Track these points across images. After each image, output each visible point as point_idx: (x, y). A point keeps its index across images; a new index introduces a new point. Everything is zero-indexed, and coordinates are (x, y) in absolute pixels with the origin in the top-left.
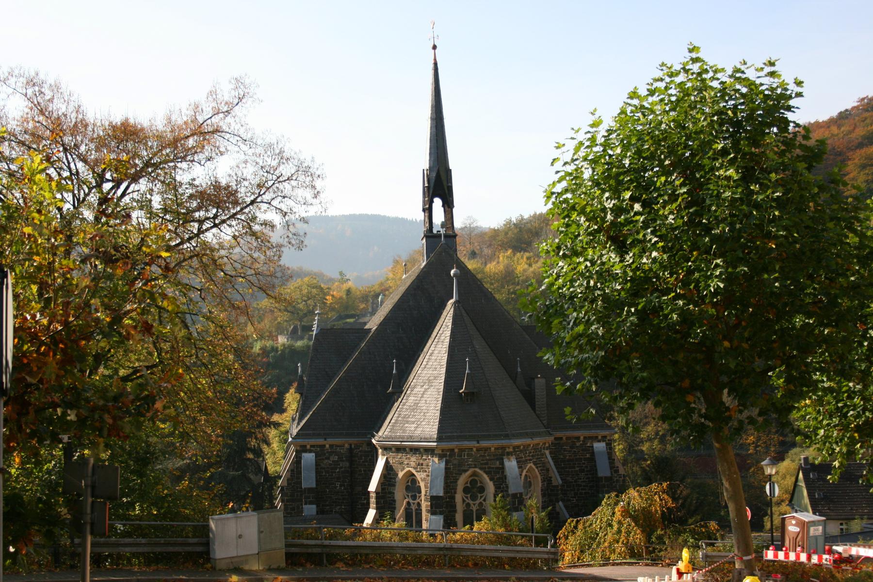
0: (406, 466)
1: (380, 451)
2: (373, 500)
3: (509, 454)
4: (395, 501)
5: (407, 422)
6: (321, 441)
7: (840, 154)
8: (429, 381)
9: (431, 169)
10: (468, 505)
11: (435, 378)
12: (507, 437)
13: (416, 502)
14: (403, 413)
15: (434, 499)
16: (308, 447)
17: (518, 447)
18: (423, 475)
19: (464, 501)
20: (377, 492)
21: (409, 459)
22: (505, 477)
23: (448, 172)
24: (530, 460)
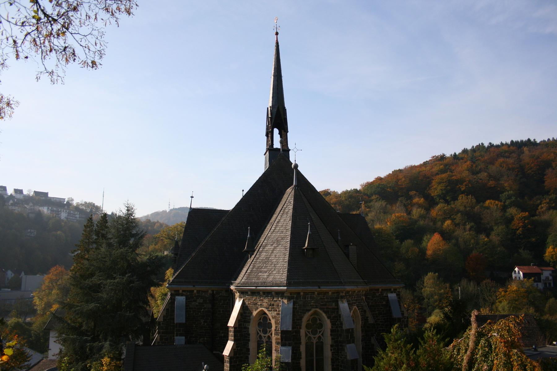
0: (261, 306)
1: (237, 295)
2: (231, 334)
3: (342, 297)
4: (249, 335)
5: (261, 272)
6: (190, 287)
7: (428, 178)
8: (277, 241)
9: (273, 107)
10: (310, 338)
11: (282, 239)
12: (341, 284)
13: (267, 335)
14: (257, 265)
15: (284, 333)
16: (181, 291)
17: (348, 292)
18: (274, 313)
19: (306, 335)
20: (235, 327)
21: (262, 300)
22: (340, 316)
23: (285, 110)
24: (355, 303)
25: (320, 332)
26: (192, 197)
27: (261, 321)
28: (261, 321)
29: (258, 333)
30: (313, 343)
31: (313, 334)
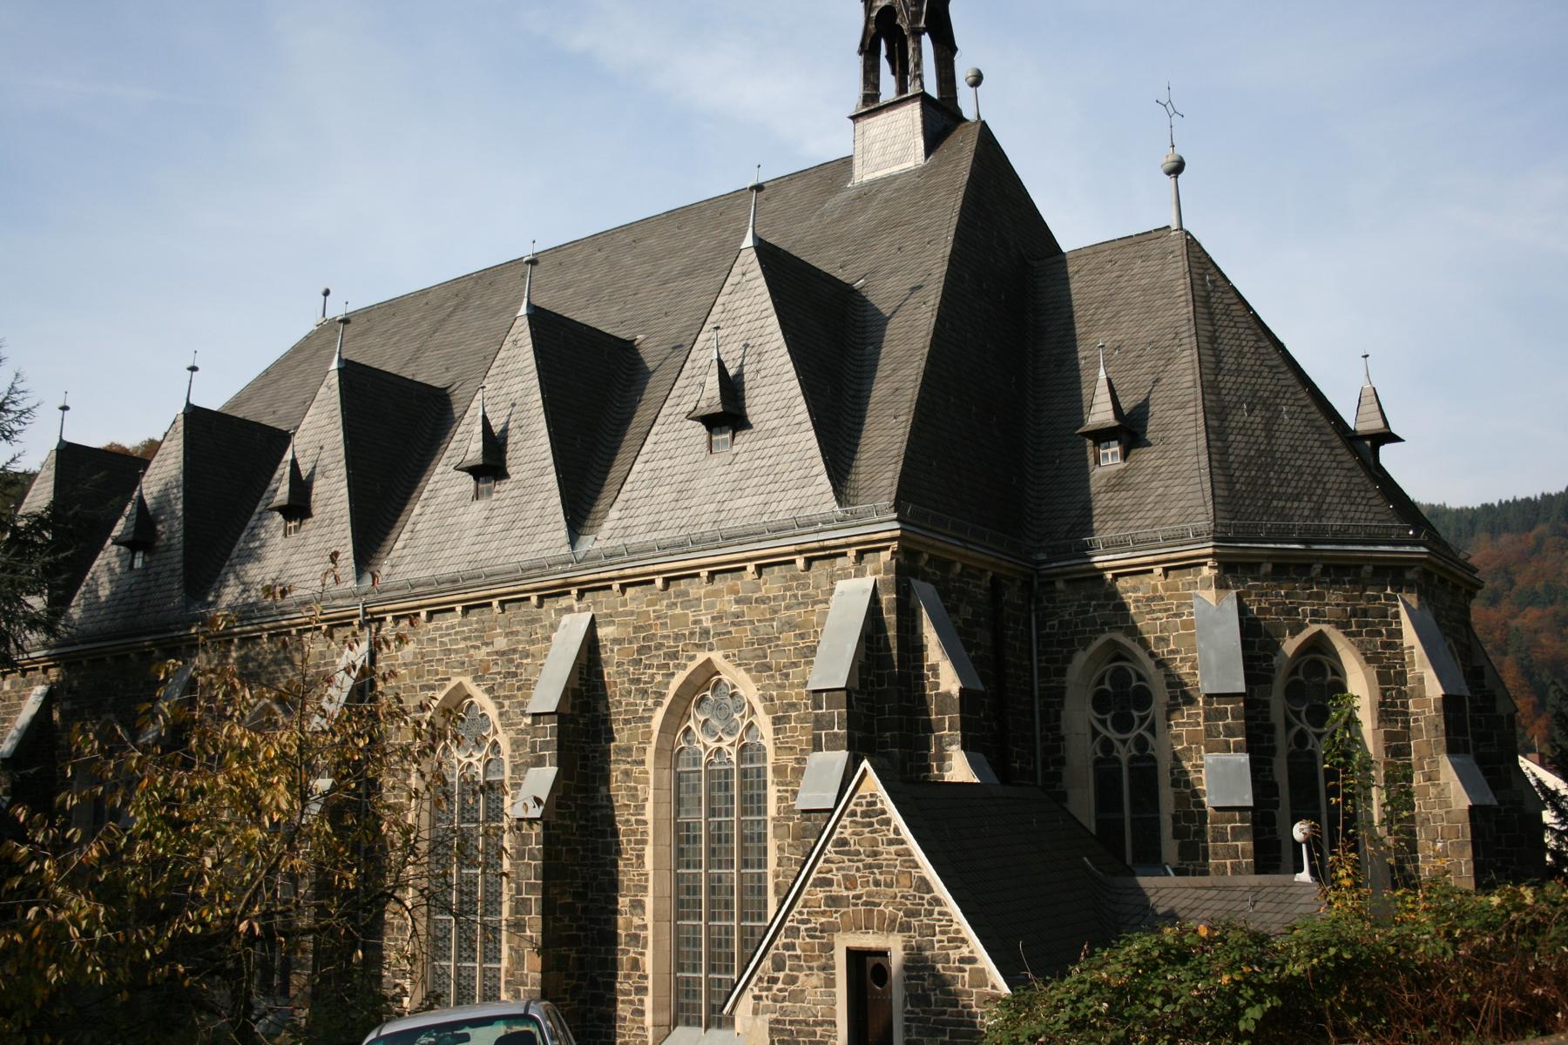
10: (1107, 745)
13: (1132, 735)
21: (1320, 596)
25: (1143, 719)
26: (193, 369)
27: (1107, 686)
28: (1107, 686)
29: (1095, 733)
30: (1117, 760)
31: (1120, 731)
